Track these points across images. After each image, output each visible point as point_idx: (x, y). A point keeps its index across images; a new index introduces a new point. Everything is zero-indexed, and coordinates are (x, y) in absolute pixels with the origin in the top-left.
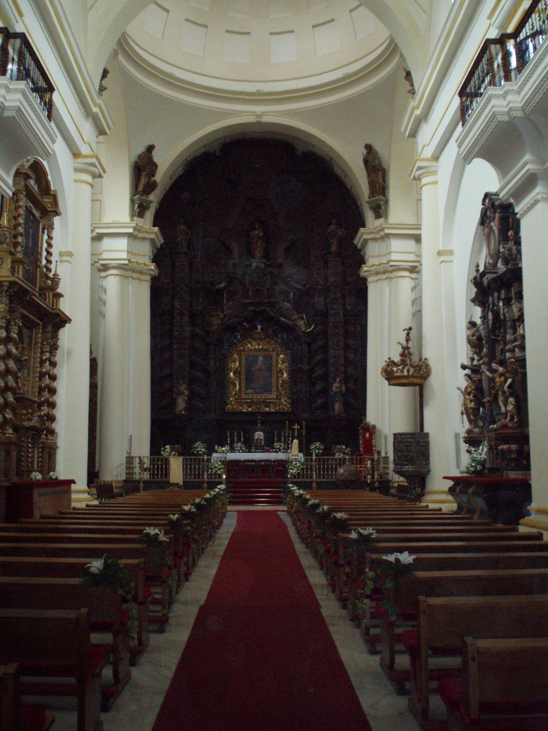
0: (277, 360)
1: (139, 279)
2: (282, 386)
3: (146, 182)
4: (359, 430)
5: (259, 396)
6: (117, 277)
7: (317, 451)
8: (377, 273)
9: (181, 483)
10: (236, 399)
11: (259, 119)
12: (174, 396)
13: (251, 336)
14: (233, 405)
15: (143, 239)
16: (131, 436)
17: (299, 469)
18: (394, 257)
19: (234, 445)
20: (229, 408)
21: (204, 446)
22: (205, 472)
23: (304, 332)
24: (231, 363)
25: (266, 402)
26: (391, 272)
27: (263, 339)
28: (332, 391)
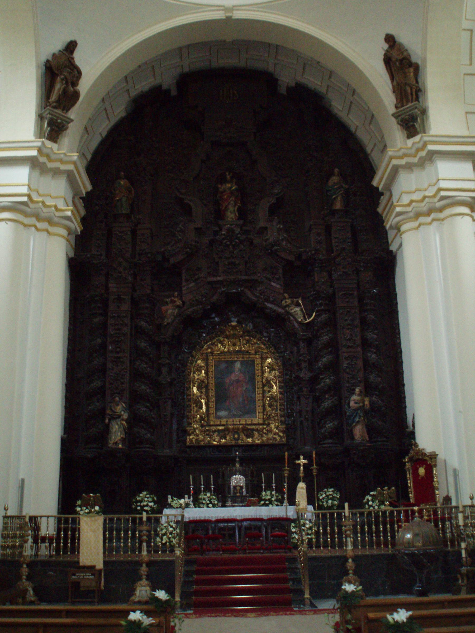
0: (262, 367)
1: (47, 231)
2: (270, 406)
3: (61, 90)
4: (405, 463)
5: (236, 421)
6: (9, 223)
7: (330, 502)
8: (418, 215)
9: (100, 565)
10: (202, 426)
11: (229, 14)
12: (107, 421)
13: (222, 332)
14: (197, 435)
15: (56, 172)
16: (23, 480)
17: (310, 532)
18: (443, 184)
19: (200, 497)
20: (191, 440)
21: (153, 498)
22: (144, 544)
23: (300, 323)
24: (194, 373)
25: (248, 429)
26: (441, 210)
27: (241, 336)
28: (349, 407)
